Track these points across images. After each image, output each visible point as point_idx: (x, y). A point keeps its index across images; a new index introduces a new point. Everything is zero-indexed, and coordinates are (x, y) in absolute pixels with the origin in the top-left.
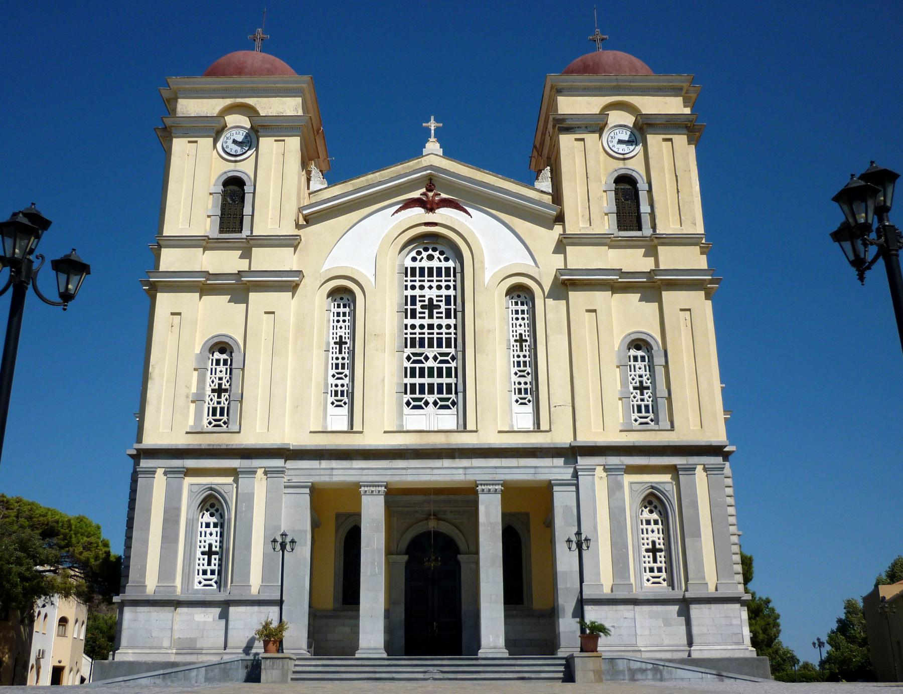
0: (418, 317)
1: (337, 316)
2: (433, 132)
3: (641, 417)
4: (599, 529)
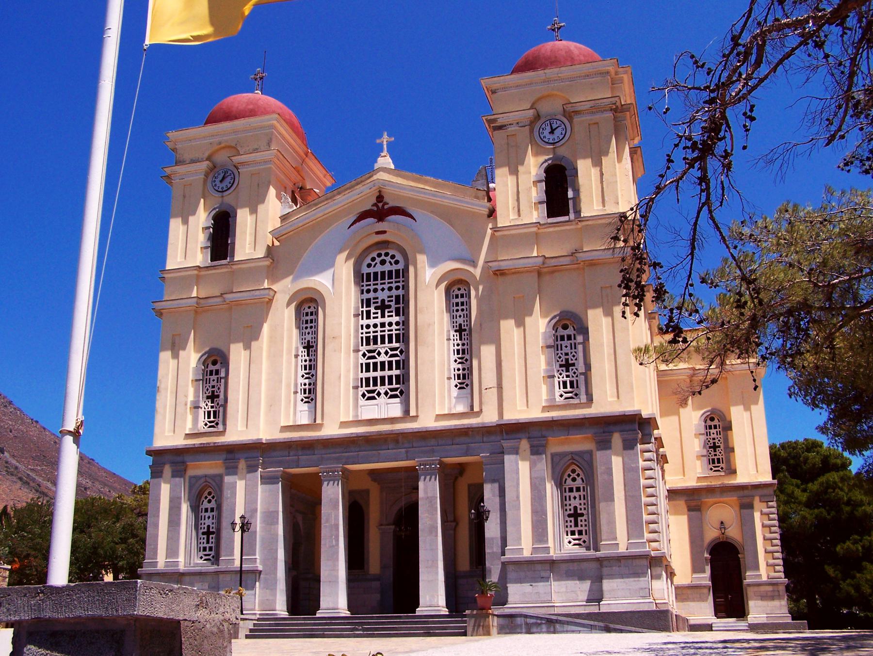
0: (372, 318)
1: (456, 306)
2: (385, 146)
3: (566, 393)
4: (521, 498)
